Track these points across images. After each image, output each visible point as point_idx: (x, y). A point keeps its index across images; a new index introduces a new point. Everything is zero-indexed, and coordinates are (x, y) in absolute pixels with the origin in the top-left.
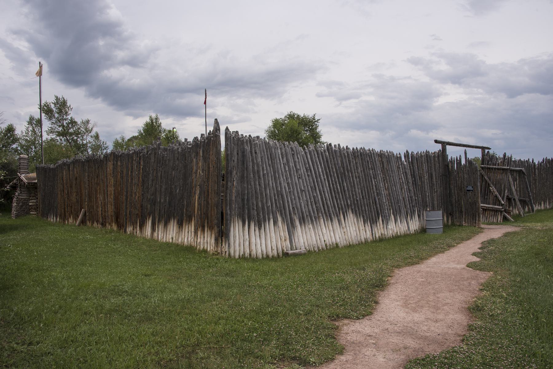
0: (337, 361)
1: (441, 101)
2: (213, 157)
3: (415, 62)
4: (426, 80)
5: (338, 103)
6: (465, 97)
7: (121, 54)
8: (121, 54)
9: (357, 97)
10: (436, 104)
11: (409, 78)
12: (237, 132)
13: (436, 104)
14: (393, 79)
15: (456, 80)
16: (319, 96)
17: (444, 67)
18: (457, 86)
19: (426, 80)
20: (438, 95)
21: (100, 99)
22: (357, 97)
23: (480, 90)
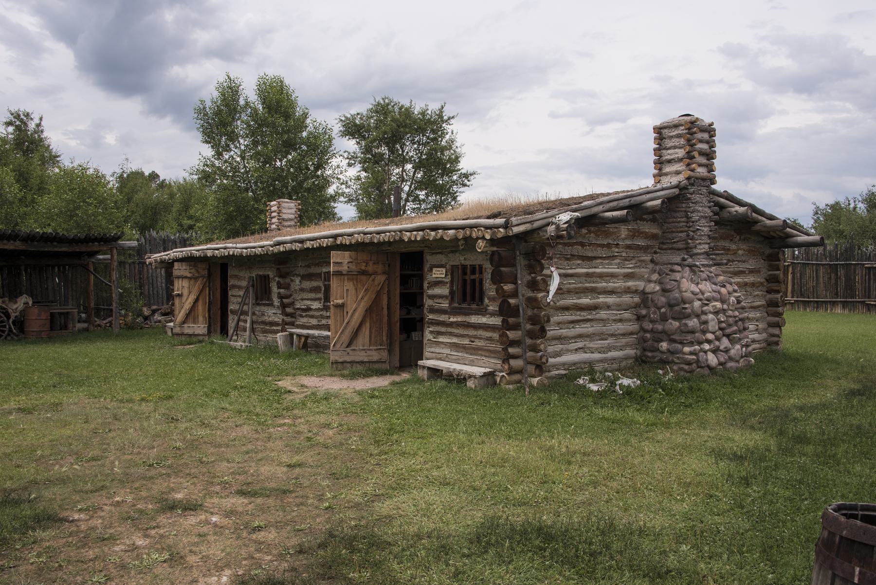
0: (321, 523)
1: (768, 127)
2: (555, 212)
3: (732, 52)
4: (747, 86)
5: (587, 129)
6: (816, 119)
7: (203, 37)
8: (203, 37)
9: (623, 119)
10: (761, 132)
11: (721, 81)
12: (654, 150)
13: (761, 132)
14: (689, 84)
15: (805, 86)
16: (554, 116)
17: (782, 62)
18: (804, 96)
19: (747, 86)
20: (767, 115)
21: (168, 119)
22: (623, 119)
23: (849, 105)
